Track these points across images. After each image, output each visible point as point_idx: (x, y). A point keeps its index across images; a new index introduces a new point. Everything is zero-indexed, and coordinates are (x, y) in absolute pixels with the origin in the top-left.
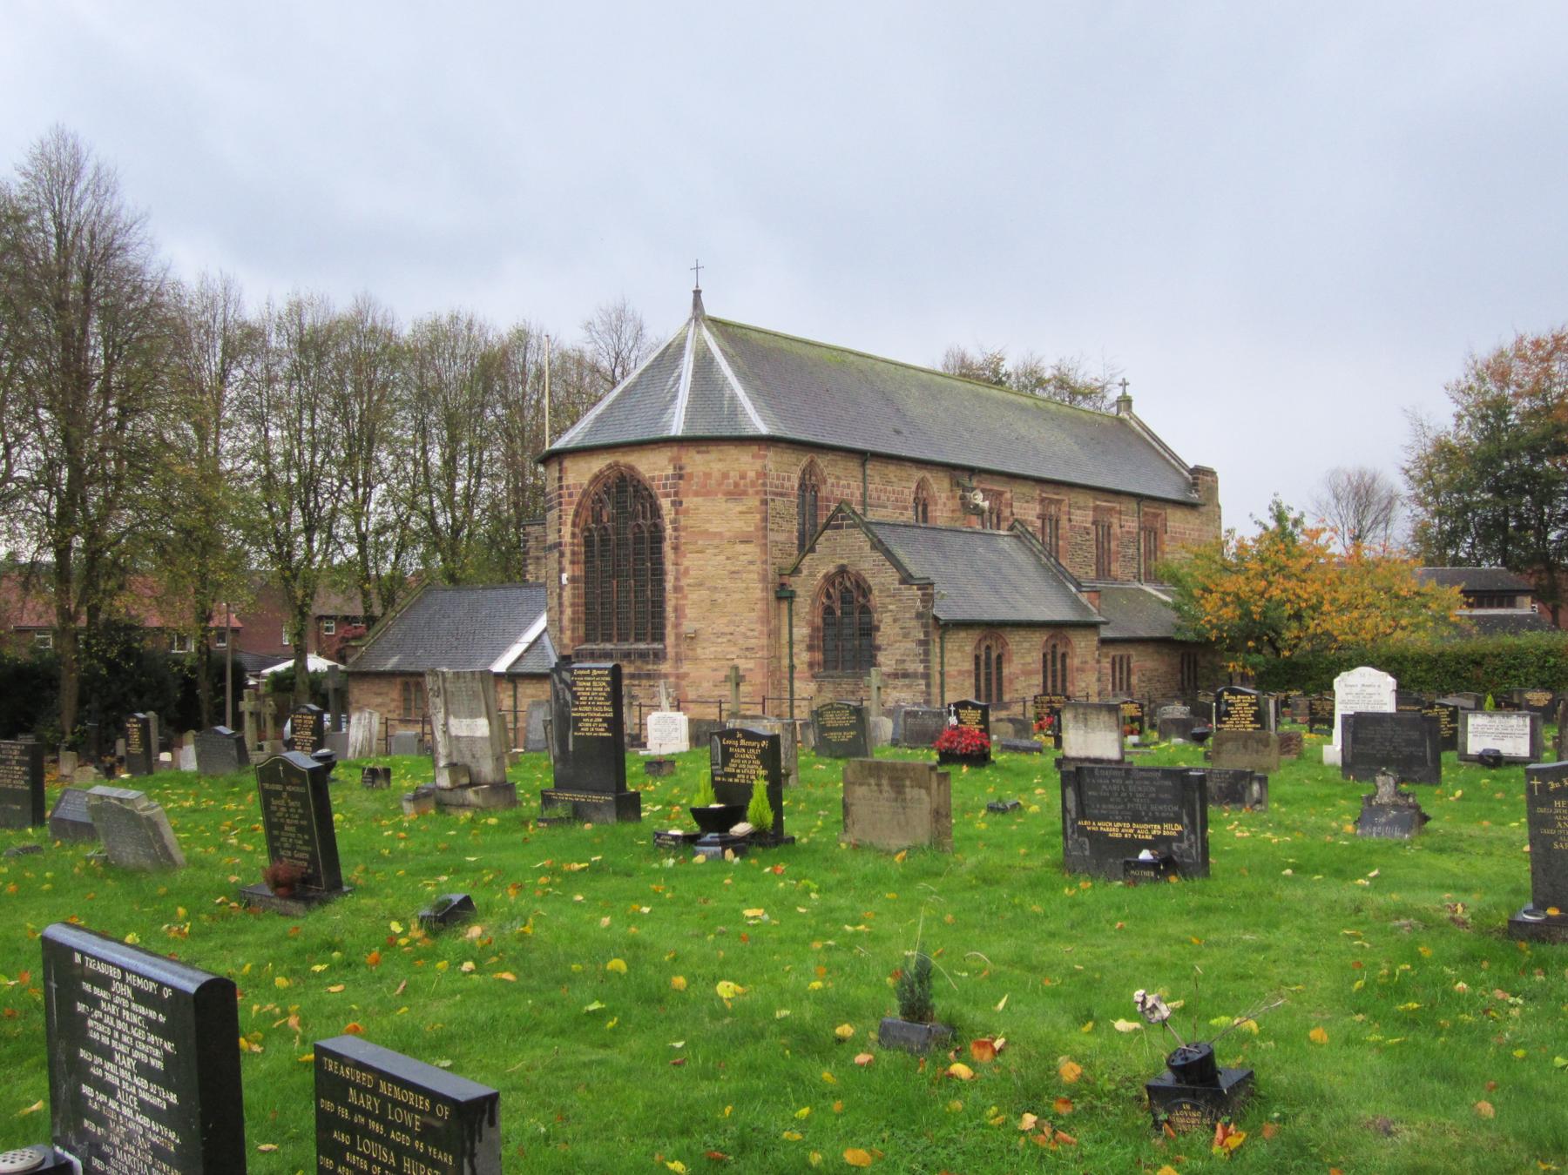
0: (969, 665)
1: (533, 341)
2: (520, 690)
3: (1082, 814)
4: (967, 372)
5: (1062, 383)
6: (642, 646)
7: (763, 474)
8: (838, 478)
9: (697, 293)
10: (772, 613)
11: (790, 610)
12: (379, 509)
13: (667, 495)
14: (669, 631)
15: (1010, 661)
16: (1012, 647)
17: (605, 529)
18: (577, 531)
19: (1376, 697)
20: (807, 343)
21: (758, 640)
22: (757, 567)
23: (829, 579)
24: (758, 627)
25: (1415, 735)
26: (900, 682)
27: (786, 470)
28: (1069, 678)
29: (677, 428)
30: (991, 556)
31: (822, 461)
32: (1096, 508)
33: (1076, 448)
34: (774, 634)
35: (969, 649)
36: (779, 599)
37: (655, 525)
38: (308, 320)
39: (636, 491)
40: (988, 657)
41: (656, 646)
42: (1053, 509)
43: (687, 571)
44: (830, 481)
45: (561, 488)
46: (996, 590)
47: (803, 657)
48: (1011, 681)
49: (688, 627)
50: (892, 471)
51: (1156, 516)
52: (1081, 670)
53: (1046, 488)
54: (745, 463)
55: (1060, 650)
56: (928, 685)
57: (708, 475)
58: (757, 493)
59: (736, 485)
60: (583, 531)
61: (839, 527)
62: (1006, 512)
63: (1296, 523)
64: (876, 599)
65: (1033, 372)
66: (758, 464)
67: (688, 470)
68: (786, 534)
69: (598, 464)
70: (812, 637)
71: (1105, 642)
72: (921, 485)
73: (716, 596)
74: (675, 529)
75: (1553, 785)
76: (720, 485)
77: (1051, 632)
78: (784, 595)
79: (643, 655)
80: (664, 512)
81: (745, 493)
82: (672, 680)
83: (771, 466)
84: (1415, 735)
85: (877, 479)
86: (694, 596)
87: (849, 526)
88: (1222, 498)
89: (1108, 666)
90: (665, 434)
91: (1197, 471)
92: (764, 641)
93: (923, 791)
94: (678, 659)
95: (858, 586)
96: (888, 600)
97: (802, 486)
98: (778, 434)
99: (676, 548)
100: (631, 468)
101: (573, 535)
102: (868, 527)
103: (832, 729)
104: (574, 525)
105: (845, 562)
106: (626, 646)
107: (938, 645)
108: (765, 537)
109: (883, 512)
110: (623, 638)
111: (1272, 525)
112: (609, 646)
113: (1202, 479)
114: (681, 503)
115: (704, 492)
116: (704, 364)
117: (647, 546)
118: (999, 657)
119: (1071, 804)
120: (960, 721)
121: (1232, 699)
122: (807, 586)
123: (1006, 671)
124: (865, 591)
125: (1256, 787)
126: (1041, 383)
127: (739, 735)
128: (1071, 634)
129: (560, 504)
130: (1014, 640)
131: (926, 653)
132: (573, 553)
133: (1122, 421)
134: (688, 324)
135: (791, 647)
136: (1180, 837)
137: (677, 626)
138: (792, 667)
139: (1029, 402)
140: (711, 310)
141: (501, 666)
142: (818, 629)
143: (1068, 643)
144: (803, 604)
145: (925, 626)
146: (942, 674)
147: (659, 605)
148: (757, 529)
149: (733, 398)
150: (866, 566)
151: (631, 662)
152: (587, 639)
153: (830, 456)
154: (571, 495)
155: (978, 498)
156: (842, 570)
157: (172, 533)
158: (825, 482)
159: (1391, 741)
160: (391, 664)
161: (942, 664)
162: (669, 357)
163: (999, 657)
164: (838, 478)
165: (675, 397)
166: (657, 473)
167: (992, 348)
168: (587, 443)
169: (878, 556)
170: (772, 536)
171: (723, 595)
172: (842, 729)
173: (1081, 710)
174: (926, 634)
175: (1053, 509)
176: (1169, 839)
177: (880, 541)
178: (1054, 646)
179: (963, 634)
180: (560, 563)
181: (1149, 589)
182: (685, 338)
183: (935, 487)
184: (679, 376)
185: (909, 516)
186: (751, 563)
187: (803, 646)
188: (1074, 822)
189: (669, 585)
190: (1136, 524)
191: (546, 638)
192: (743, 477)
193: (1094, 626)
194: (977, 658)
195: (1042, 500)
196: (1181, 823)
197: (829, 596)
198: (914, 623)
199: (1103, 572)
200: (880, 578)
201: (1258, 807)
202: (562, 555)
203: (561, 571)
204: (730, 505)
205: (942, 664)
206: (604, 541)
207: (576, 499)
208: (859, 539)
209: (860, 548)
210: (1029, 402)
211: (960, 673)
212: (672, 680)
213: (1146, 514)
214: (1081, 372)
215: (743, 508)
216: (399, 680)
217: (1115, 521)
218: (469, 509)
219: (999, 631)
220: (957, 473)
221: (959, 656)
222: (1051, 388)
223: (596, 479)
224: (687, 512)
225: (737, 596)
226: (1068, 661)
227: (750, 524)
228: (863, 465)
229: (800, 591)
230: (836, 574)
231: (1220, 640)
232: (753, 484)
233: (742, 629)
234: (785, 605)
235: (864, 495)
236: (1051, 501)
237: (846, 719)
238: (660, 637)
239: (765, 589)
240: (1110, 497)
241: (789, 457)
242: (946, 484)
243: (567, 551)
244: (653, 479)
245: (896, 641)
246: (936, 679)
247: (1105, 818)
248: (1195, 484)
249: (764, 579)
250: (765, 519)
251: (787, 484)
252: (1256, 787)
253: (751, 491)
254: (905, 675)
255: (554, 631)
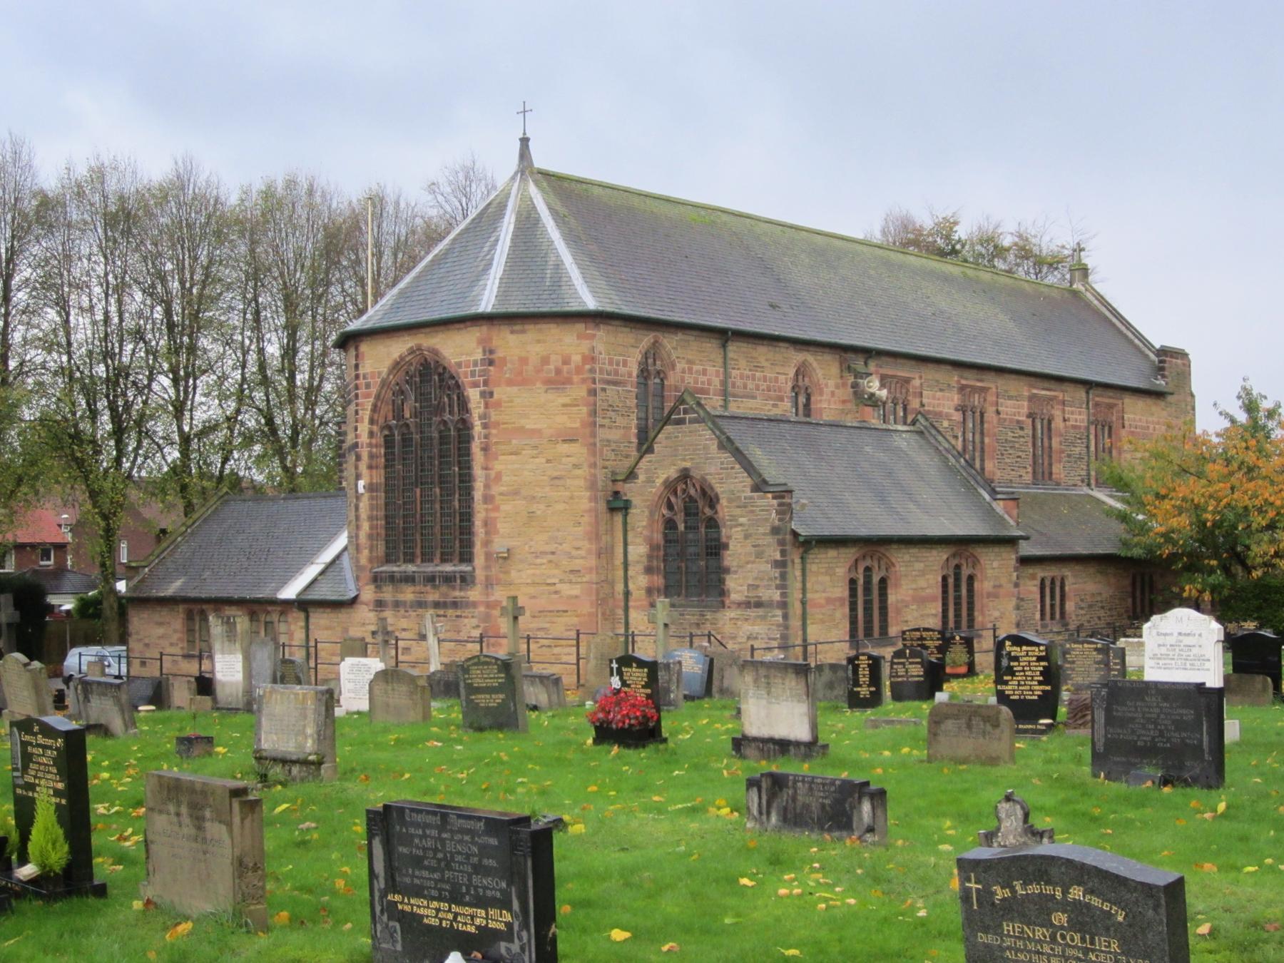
0: (842, 591)
1: (390, 209)
2: (312, 620)
3: (392, 886)
4: (913, 241)
5: (1025, 252)
6: (448, 568)
7: (591, 359)
8: (690, 362)
9: (525, 141)
10: (602, 528)
11: (625, 524)
12: (205, 410)
13: (475, 385)
14: (478, 550)
15: (897, 586)
16: (900, 568)
17: (407, 425)
18: (375, 428)
19: (1195, 651)
20: (668, 200)
21: (585, 559)
22: (584, 472)
23: (671, 486)
24: (586, 544)
25: (1188, 714)
26: (752, 613)
27: (623, 353)
28: (977, 606)
29: (487, 302)
30: (881, 456)
31: (670, 343)
32: (1032, 398)
33: (1011, 325)
34: (604, 553)
35: (842, 571)
36: (612, 510)
37: (464, 421)
38: (112, 185)
39: (441, 380)
40: (868, 582)
41: (465, 568)
42: (976, 400)
43: (499, 477)
44: (680, 366)
45: (357, 377)
46: (882, 498)
47: (640, 582)
48: (898, 611)
49: (499, 545)
50: (762, 353)
51: (1111, 406)
52: (993, 595)
53: (968, 373)
54: (569, 344)
55: (965, 572)
56: (785, 617)
57: (524, 361)
58: (584, 381)
59: (558, 371)
60: (382, 429)
61: (680, 422)
62: (914, 404)
63: (1271, 414)
64: (725, 510)
65: (989, 240)
66: (585, 346)
67: (499, 354)
68: (623, 429)
69: (398, 348)
70: (650, 557)
71: (1025, 561)
72: (801, 372)
73: (534, 507)
74: (485, 426)
75: (1000, 893)
76: (538, 371)
77: (952, 550)
78: (618, 505)
79: (448, 579)
80: (472, 405)
81: (569, 381)
82: (482, 609)
83: (600, 347)
84: (1188, 714)
85: (743, 363)
86: (506, 507)
87: (692, 421)
88: (1196, 385)
89: (1036, 590)
90: (473, 311)
91: (1164, 352)
92: (592, 562)
93: (224, 828)
94: (489, 584)
95: (704, 493)
96: (738, 511)
97: (644, 373)
98: (609, 308)
99: (485, 449)
100: (435, 352)
101: (371, 434)
102: (714, 421)
103: (479, 690)
104: (372, 422)
105: (688, 465)
106: (430, 568)
107: (798, 566)
108: (594, 435)
109: (751, 403)
110: (427, 558)
111: (1242, 417)
112: (411, 568)
113: (1170, 362)
114: (491, 394)
115: (520, 380)
116: (528, 225)
117: (453, 447)
118: (883, 581)
119: (379, 867)
120: (624, 683)
121: (1015, 651)
122: (644, 494)
123: (892, 598)
124: (712, 501)
125: (866, 807)
126: (1000, 252)
127: (36, 729)
128: (980, 551)
129: (357, 396)
130: (903, 561)
131: (783, 576)
132: (371, 456)
133: (1076, 294)
134: (513, 178)
135: (626, 570)
136: (508, 935)
137: (487, 543)
138: (627, 594)
139: (986, 276)
140: (540, 160)
141: (290, 592)
142: (658, 547)
143: (975, 562)
144: (640, 517)
145: (782, 543)
146: (803, 603)
147: (467, 517)
148: (583, 425)
149: (559, 266)
150: (713, 470)
151: (434, 587)
152: (388, 559)
153: (680, 336)
154: (368, 386)
155: (874, 386)
156: (685, 476)
157: (868, 449)
158: (673, 367)
159: (1155, 723)
160: (173, 588)
161: (804, 590)
162: (489, 218)
163: (883, 581)
164: (690, 362)
165: (489, 265)
166: (464, 358)
167: (943, 212)
168: (386, 323)
169: (727, 457)
170: (602, 434)
171: (542, 507)
172: (490, 690)
173: (762, 672)
174: (783, 553)
175: (976, 400)
176: (495, 935)
177: (728, 438)
178: (958, 567)
179: (832, 553)
180: (356, 468)
181: (1101, 495)
182: (508, 196)
183: (820, 373)
184: (497, 241)
185: (785, 408)
186: (576, 466)
187: (640, 567)
188: (384, 894)
189: (478, 494)
190: (1084, 417)
191: (346, 560)
192: (566, 361)
193: (1011, 542)
194: (853, 582)
195: (962, 389)
196: (510, 910)
197: (670, 506)
198: (770, 539)
199: (1042, 474)
200: (730, 484)
201: (869, 837)
202: (358, 458)
203: (358, 477)
204: (550, 396)
205: (804, 590)
206: (406, 441)
207: (374, 390)
208: (705, 436)
209: (706, 448)
210: (986, 276)
211: (829, 601)
212: (482, 609)
213: (1097, 405)
214: (1046, 239)
215: (567, 400)
216: (181, 608)
217: (1057, 413)
218: (311, 404)
219: (882, 549)
220: (850, 355)
221: (828, 579)
222: (1011, 258)
223: (396, 366)
224: (498, 404)
225: (560, 507)
226: (976, 585)
227: (574, 419)
228: (724, 346)
229: (636, 501)
230: (678, 480)
231: (1173, 557)
232: (579, 370)
233: (566, 547)
234: (618, 518)
235: (724, 383)
236: (974, 390)
237: (493, 677)
238: (467, 557)
239: (594, 499)
240: (1052, 385)
241: (626, 336)
242: (834, 369)
243: (365, 453)
244: (459, 364)
245: (748, 561)
246: (796, 608)
247: (418, 892)
248: (1162, 369)
249: (592, 485)
250: (594, 413)
251: (622, 369)
252: (866, 807)
253: (576, 378)
254: (759, 605)
255: (352, 550)
